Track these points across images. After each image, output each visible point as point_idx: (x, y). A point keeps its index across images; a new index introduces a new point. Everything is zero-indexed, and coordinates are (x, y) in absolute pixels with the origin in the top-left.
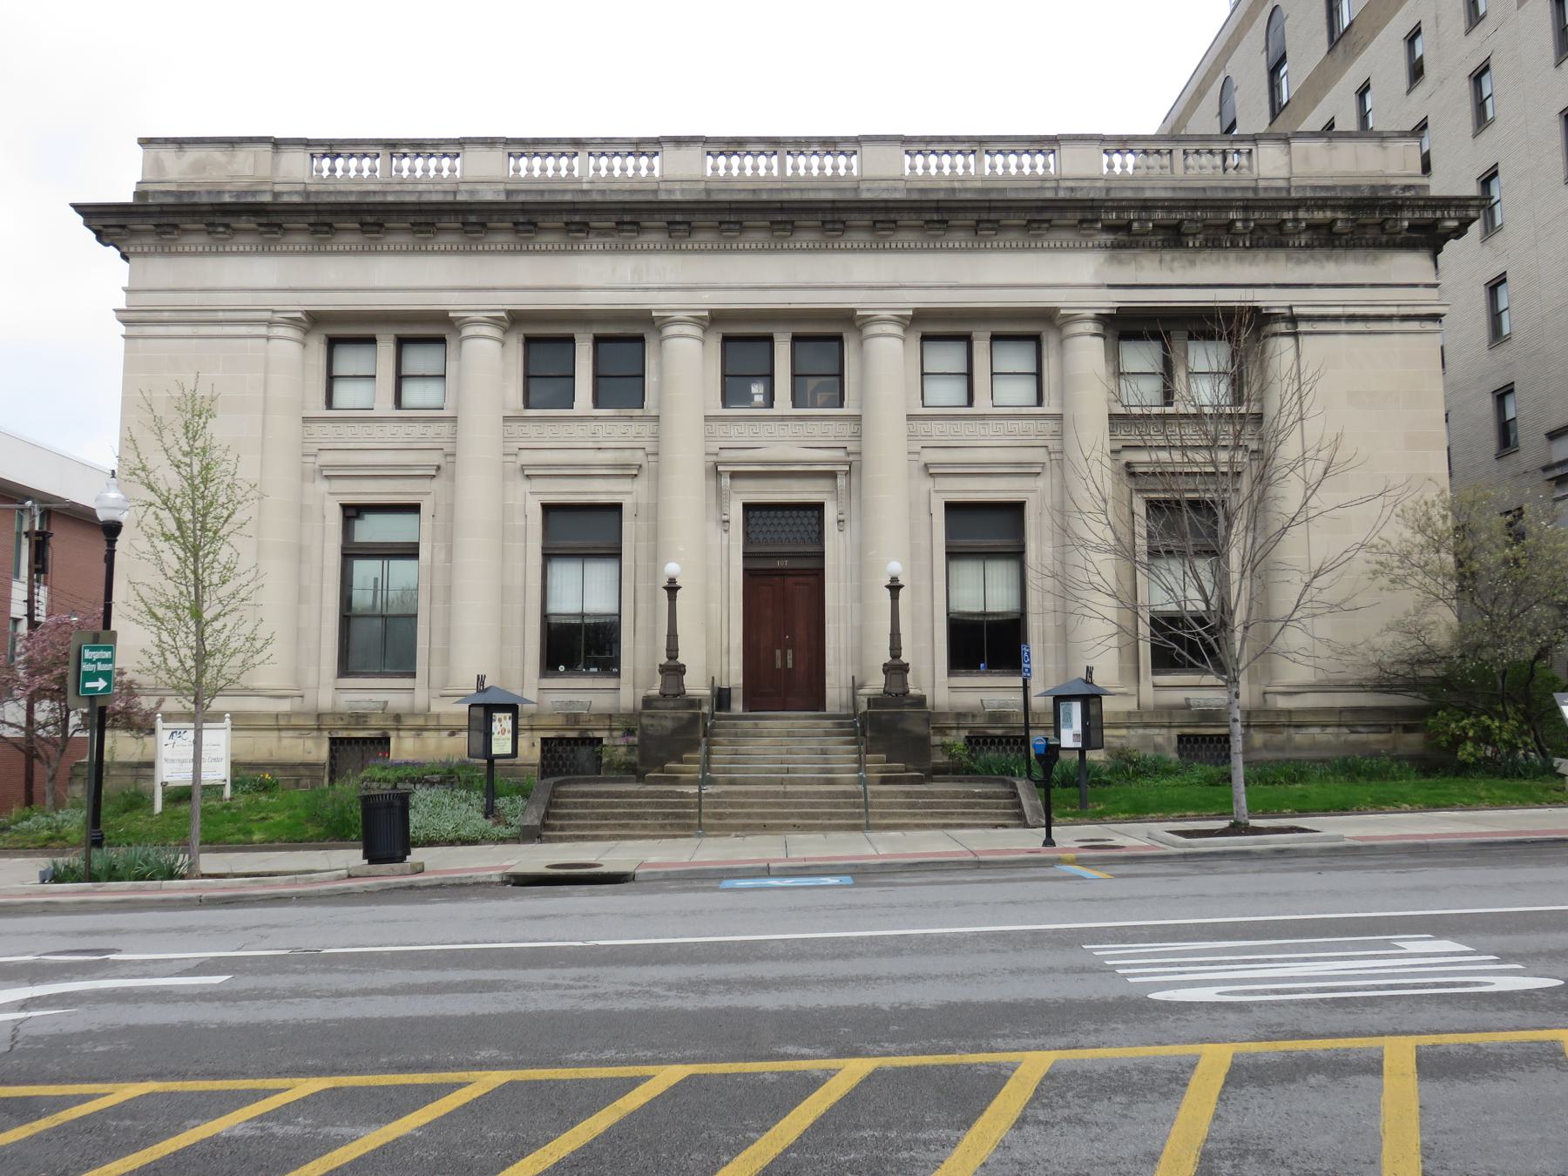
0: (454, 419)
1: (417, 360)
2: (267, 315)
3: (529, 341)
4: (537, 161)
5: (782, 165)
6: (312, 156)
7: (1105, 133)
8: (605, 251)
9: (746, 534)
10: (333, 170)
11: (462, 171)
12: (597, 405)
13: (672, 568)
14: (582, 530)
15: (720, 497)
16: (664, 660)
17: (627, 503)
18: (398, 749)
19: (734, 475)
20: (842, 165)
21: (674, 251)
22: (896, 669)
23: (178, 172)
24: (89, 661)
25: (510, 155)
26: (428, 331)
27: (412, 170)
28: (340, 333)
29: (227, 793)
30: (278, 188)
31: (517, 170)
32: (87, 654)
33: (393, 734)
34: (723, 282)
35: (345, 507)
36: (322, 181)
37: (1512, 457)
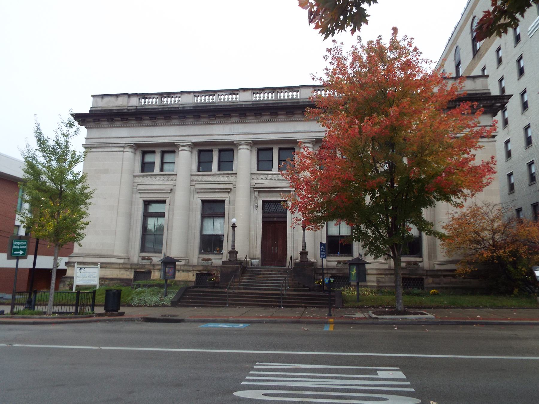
0: (176, 175)
1: (168, 158)
2: (123, 145)
3: (259, 150)
4: (203, 98)
5: (276, 96)
6: (195, 96)
7: (194, 90)
8: (221, 123)
9: (263, 210)
10: (145, 102)
11: (300, 96)
12: (258, 170)
13: (234, 220)
14: (213, 209)
15: (255, 199)
16: (301, 250)
17: (227, 200)
18: (153, 276)
19: (259, 192)
20: (294, 95)
21: (241, 123)
22: (304, 254)
23: (104, 104)
24: (16, 245)
25: (195, 96)
26: (169, 149)
27: (167, 102)
28: (144, 149)
29: (98, 288)
30: (129, 108)
31: (256, 98)
32: (15, 243)
33: (152, 271)
34: (256, 132)
35: (145, 202)
36: (142, 106)
37: (534, 185)
